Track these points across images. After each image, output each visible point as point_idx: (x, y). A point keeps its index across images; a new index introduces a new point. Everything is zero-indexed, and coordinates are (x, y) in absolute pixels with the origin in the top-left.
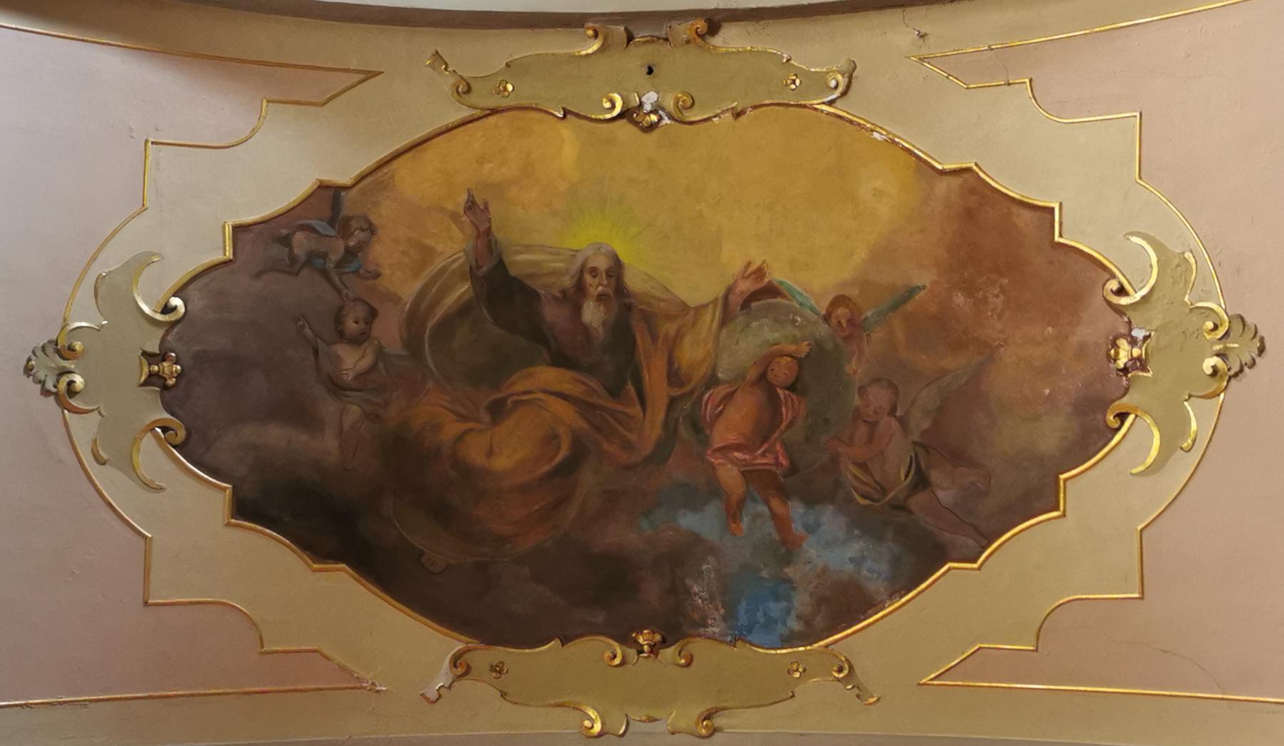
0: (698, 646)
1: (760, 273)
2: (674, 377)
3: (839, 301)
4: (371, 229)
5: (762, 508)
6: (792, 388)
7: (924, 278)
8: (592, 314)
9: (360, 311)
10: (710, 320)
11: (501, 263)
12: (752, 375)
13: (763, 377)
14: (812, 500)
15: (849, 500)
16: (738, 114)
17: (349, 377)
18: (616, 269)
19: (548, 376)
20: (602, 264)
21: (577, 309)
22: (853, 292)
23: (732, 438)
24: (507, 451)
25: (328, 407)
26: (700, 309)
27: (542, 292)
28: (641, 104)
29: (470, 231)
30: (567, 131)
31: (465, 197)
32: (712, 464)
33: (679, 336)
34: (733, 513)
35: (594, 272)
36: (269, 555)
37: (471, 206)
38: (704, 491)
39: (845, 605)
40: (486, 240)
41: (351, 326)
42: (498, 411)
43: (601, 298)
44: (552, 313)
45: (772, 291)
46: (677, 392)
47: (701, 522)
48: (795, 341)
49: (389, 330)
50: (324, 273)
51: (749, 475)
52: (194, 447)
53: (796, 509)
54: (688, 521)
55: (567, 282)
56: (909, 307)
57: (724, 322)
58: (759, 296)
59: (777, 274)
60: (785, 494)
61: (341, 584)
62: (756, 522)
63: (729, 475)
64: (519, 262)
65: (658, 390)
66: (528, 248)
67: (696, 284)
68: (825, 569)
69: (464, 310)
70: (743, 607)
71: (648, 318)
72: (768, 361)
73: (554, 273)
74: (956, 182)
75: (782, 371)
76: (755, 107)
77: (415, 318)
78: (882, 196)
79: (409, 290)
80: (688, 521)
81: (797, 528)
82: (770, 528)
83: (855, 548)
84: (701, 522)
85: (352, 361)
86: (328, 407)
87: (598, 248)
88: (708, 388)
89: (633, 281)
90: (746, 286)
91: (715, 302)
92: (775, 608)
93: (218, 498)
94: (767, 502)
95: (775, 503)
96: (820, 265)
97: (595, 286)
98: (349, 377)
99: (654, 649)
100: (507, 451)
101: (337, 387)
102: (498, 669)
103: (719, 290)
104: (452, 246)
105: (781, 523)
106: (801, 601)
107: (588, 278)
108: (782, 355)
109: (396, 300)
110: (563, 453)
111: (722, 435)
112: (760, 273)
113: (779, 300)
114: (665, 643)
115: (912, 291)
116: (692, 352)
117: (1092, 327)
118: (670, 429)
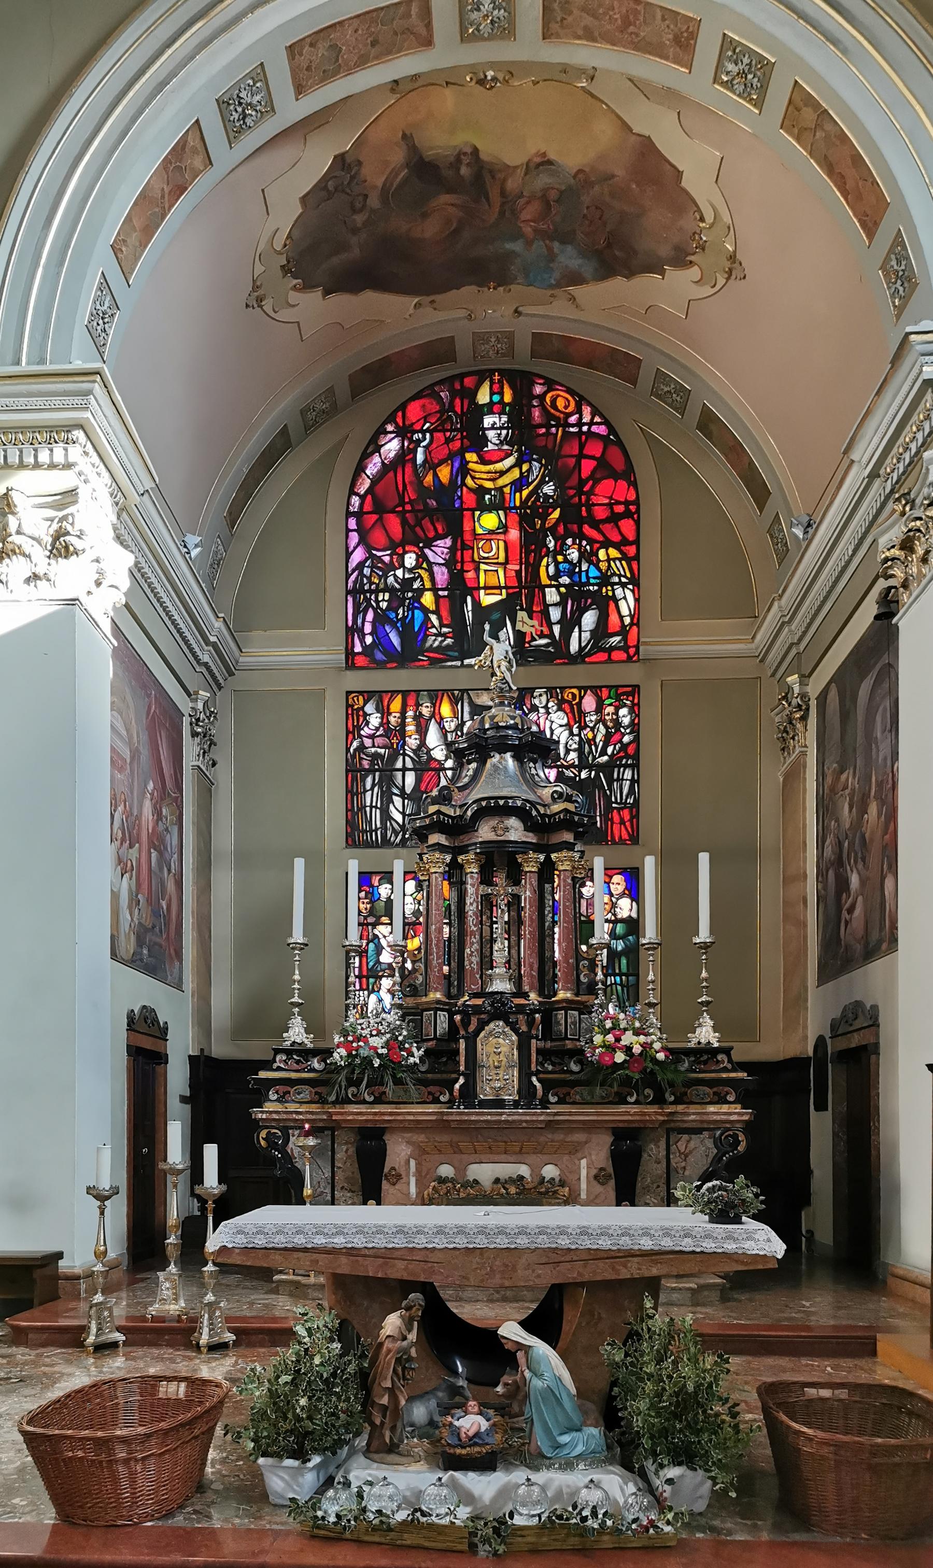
0: (512, 287)
1: (544, 154)
2: (503, 193)
3: (580, 171)
4: (360, 163)
5: (541, 243)
6: (557, 201)
7: (620, 172)
8: (464, 171)
9: (361, 198)
10: (520, 172)
11: (421, 157)
12: (540, 194)
13: (544, 196)
14: (563, 242)
15: (579, 245)
16: (535, 83)
17: (359, 225)
18: (476, 151)
19: (445, 198)
20: (469, 150)
21: (458, 169)
22: (587, 170)
23: (529, 217)
24: (430, 229)
25: (354, 240)
26: (516, 167)
27: (441, 166)
28: (486, 76)
29: (405, 147)
30: (448, 92)
31: (401, 133)
32: (520, 227)
33: (505, 180)
34: (529, 243)
35: (465, 154)
36: (342, 301)
37: (404, 136)
38: (517, 235)
39: (576, 279)
40: (413, 148)
41: (358, 205)
42: (425, 216)
43: (468, 164)
44: (447, 173)
45: (550, 162)
46: (505, 200)
47: (516, 246)
48: (559, 184)
49: (374, 201)
50: (343, 191)
51: (536, 231)
52: (307, 286)
53: (556, 245)
54: (509, 246)
55: (452, 159)
56: (610, 182)
57: (526, 174)
58: (545, 163)
59: (552, 156)
60: (552, 239)
61: (370, 297)
62: (539, 247)
63: (528, 230)
64: (429, 154)
65: (494, 194)
66: (432, 148)
67: (514, 157)
68: (566, 266)
69: (406, 181)
70: (531, 275)
71: (492, 173)
72: (546, 190)
73: (447, 156)
74: (638, 138)
75: (553, 195)
76: (545, 80)
77: (385, 190)
78: (604, 133)
79: (380, 182)
80: (509, 246)
81: (556, 250)
82: (545, 250)
83: (580, 261)
84: (516, 246)
85: (359, 219)
86: (354, 240)
87: (466, 143)
88: (519, 198)
89: (483, 156)
90: (538, 160)
91: (522, 164)
92: (546, 276)
93: (318, 294)
94: (544, 241)
95: (547, 242)
96: (573, 156)
97: (466, 160)
98: (359, 225)
99: (495, 288)
100: (430, 229)
101: (355, 231)
102: (432, 302)
103: (525, 160)
104: (398, 156)
105: (550, 249)
106: (557, 275)
107: (462, 157)
108: (553, 188)
109: (375, 187)
110: (455, 225)
111: (526, 215)
112: (544, 154)
113: (553, 167)
114: (499, 286)
115: (613, 176)
116: (512, 184)
117: (688, 223)
118: (502, 213)
